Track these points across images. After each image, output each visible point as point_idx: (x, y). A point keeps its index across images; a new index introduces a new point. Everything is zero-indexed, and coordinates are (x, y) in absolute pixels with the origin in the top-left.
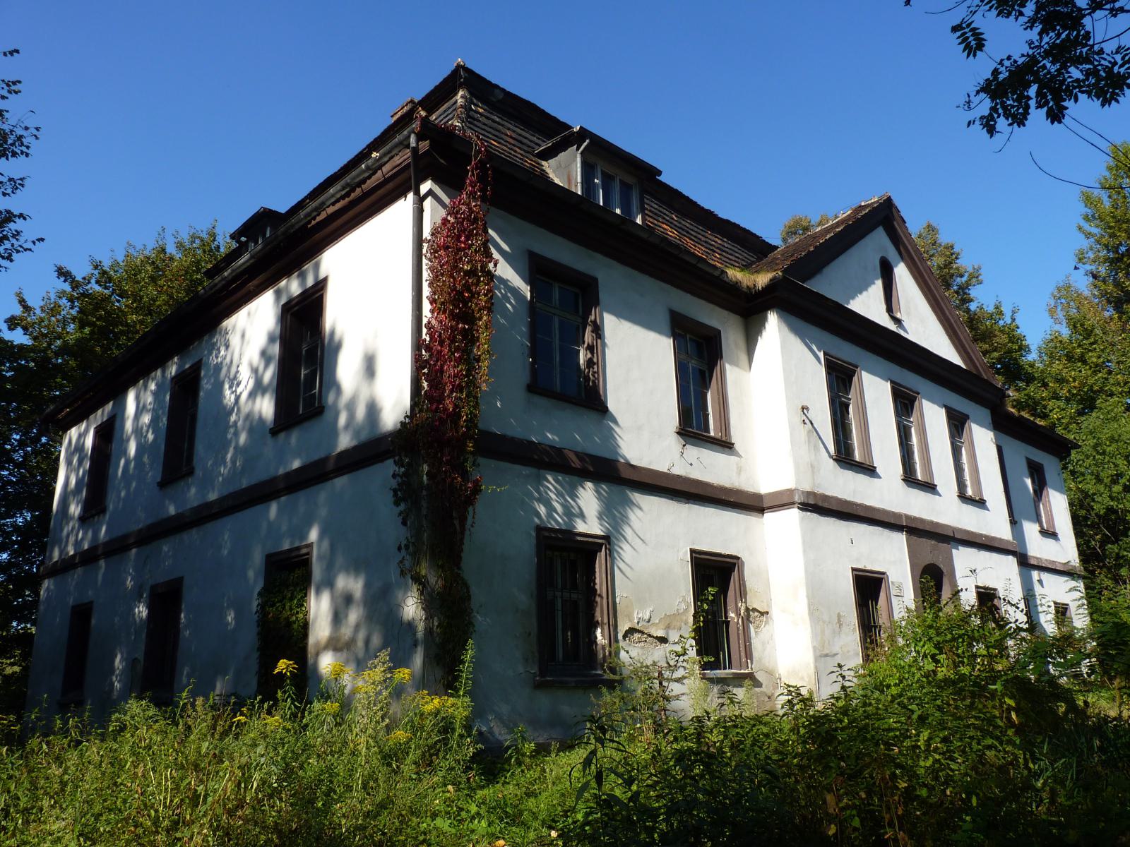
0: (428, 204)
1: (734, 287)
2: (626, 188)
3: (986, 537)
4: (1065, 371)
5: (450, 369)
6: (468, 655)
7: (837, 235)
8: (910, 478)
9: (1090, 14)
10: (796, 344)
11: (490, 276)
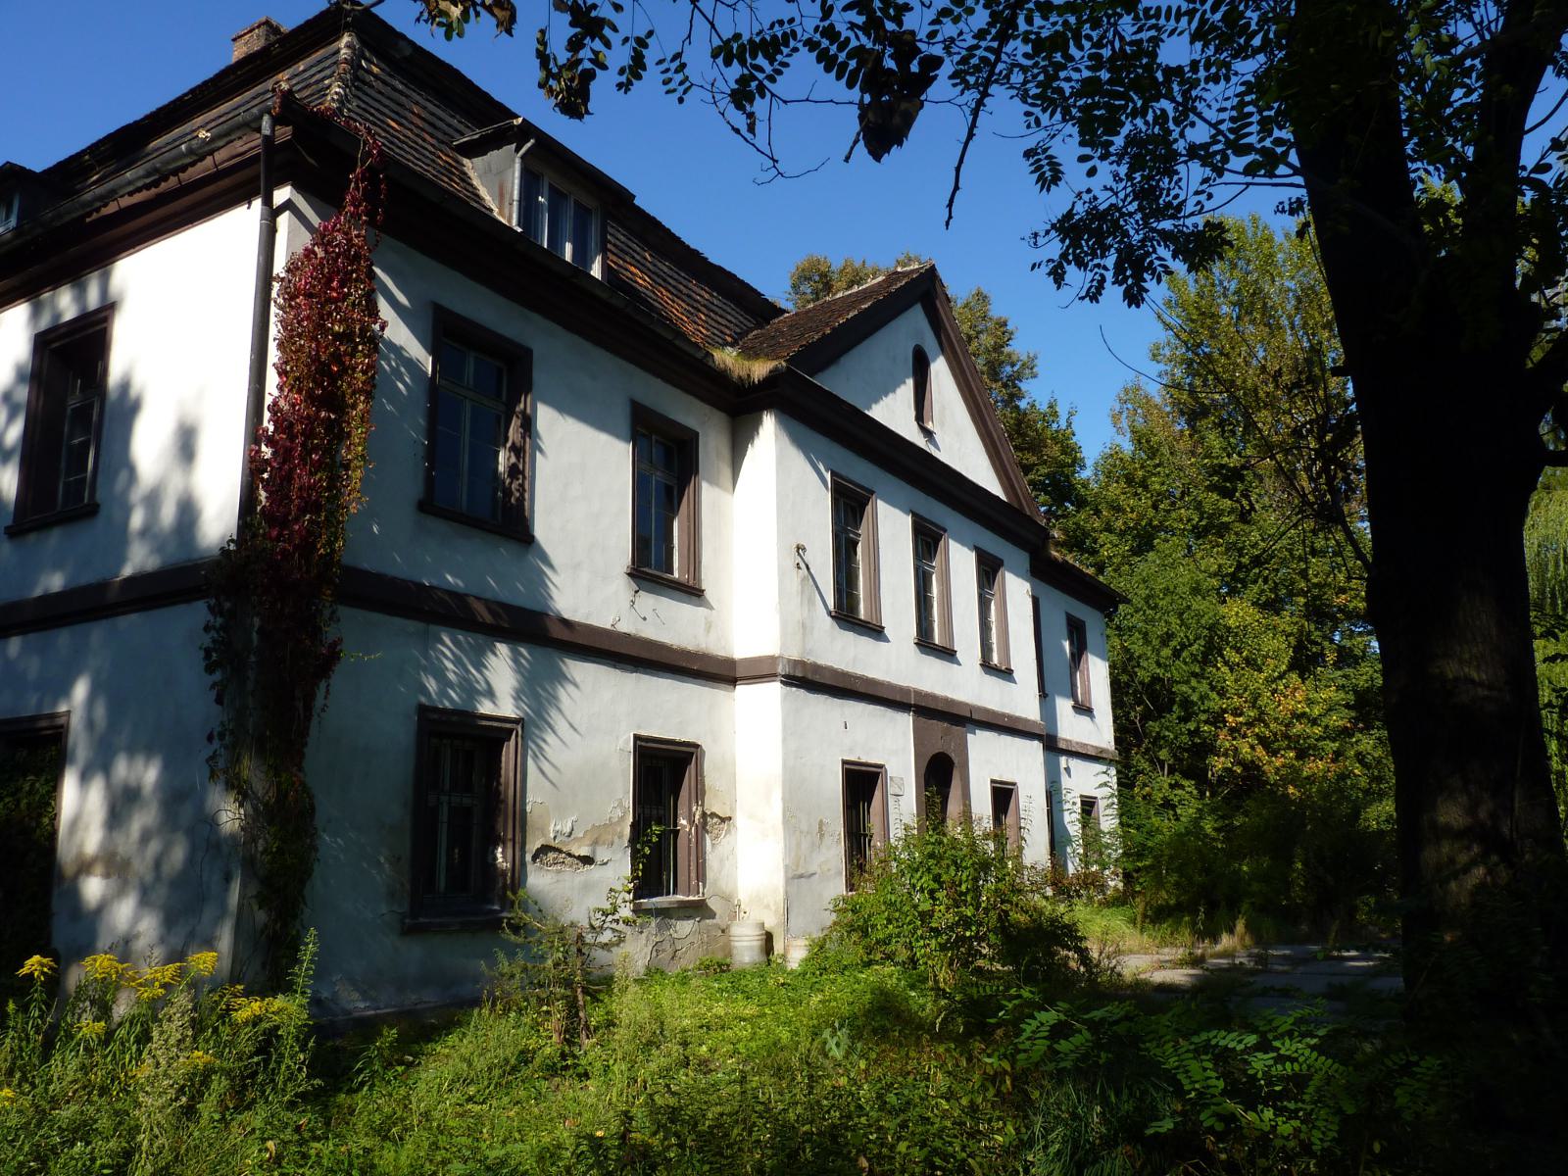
0: (284, 220)
1: (721, 377)
2: (582, 214)
3: (1010, 717)
4: (1123, 497)
5: (302, 477)
6: (309, 949)
7: (863, 313)
8: (925, 642)
9: (1185, 162)
10: (798, 461)
11: (374, 342)
